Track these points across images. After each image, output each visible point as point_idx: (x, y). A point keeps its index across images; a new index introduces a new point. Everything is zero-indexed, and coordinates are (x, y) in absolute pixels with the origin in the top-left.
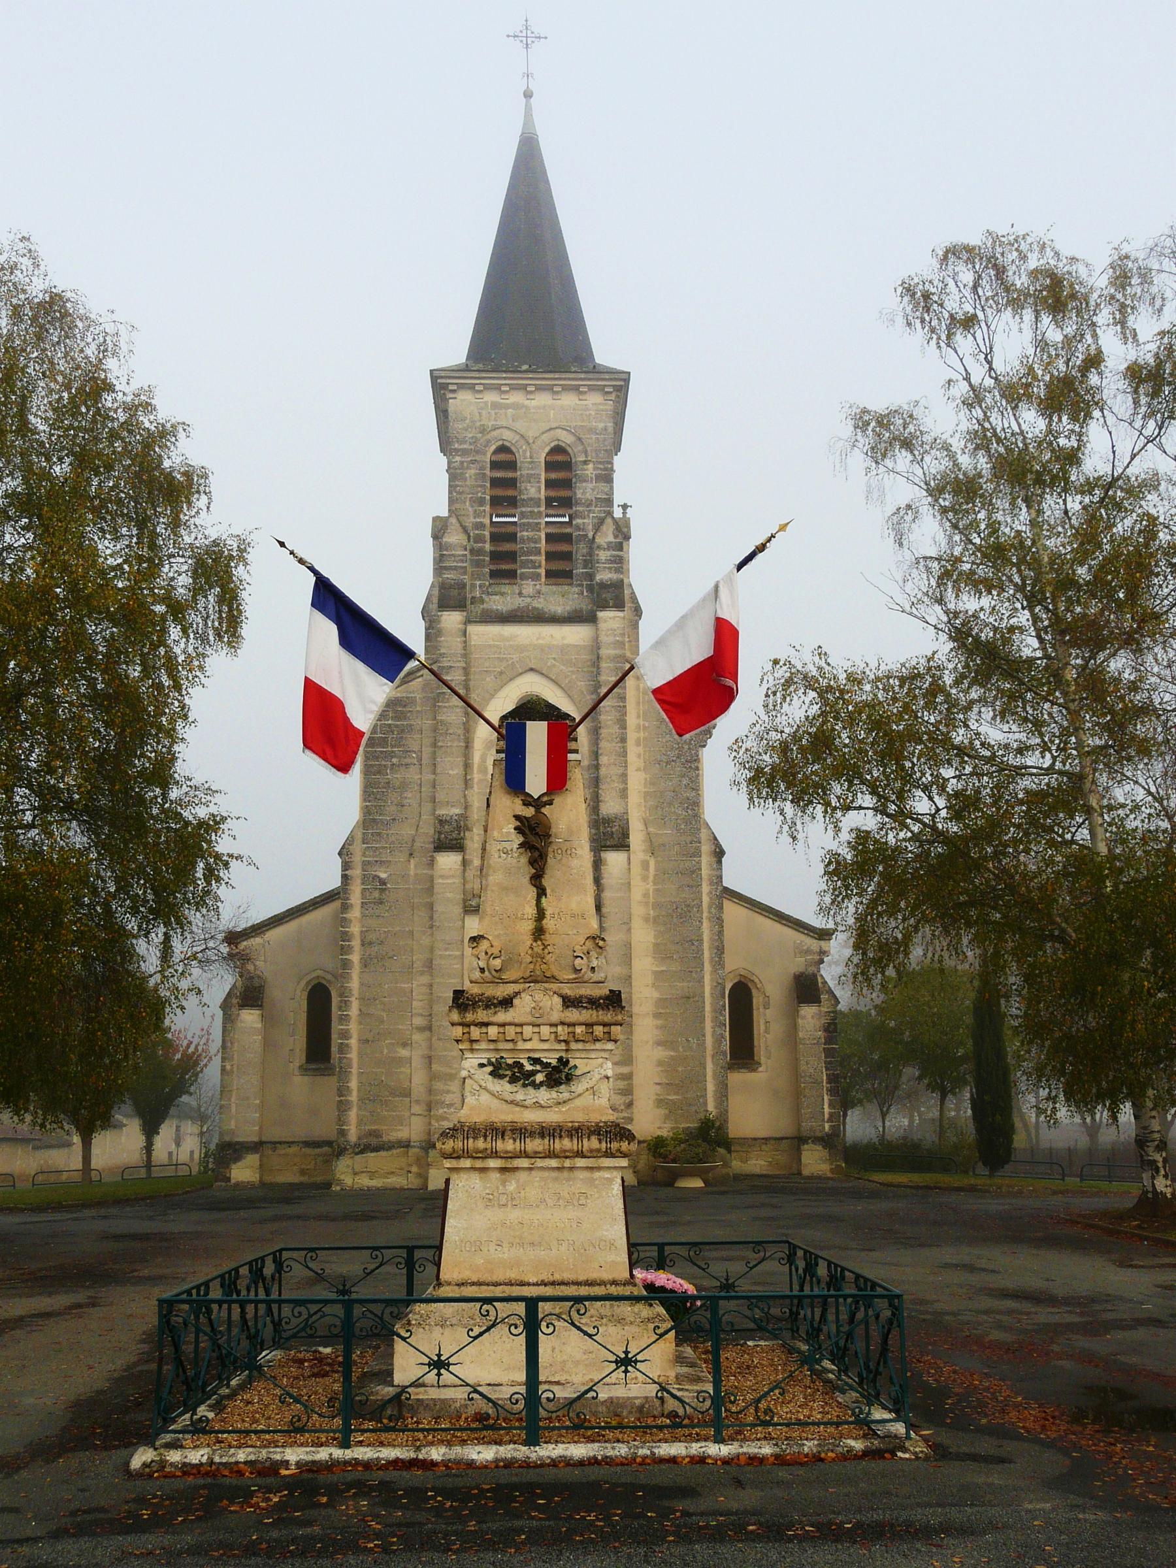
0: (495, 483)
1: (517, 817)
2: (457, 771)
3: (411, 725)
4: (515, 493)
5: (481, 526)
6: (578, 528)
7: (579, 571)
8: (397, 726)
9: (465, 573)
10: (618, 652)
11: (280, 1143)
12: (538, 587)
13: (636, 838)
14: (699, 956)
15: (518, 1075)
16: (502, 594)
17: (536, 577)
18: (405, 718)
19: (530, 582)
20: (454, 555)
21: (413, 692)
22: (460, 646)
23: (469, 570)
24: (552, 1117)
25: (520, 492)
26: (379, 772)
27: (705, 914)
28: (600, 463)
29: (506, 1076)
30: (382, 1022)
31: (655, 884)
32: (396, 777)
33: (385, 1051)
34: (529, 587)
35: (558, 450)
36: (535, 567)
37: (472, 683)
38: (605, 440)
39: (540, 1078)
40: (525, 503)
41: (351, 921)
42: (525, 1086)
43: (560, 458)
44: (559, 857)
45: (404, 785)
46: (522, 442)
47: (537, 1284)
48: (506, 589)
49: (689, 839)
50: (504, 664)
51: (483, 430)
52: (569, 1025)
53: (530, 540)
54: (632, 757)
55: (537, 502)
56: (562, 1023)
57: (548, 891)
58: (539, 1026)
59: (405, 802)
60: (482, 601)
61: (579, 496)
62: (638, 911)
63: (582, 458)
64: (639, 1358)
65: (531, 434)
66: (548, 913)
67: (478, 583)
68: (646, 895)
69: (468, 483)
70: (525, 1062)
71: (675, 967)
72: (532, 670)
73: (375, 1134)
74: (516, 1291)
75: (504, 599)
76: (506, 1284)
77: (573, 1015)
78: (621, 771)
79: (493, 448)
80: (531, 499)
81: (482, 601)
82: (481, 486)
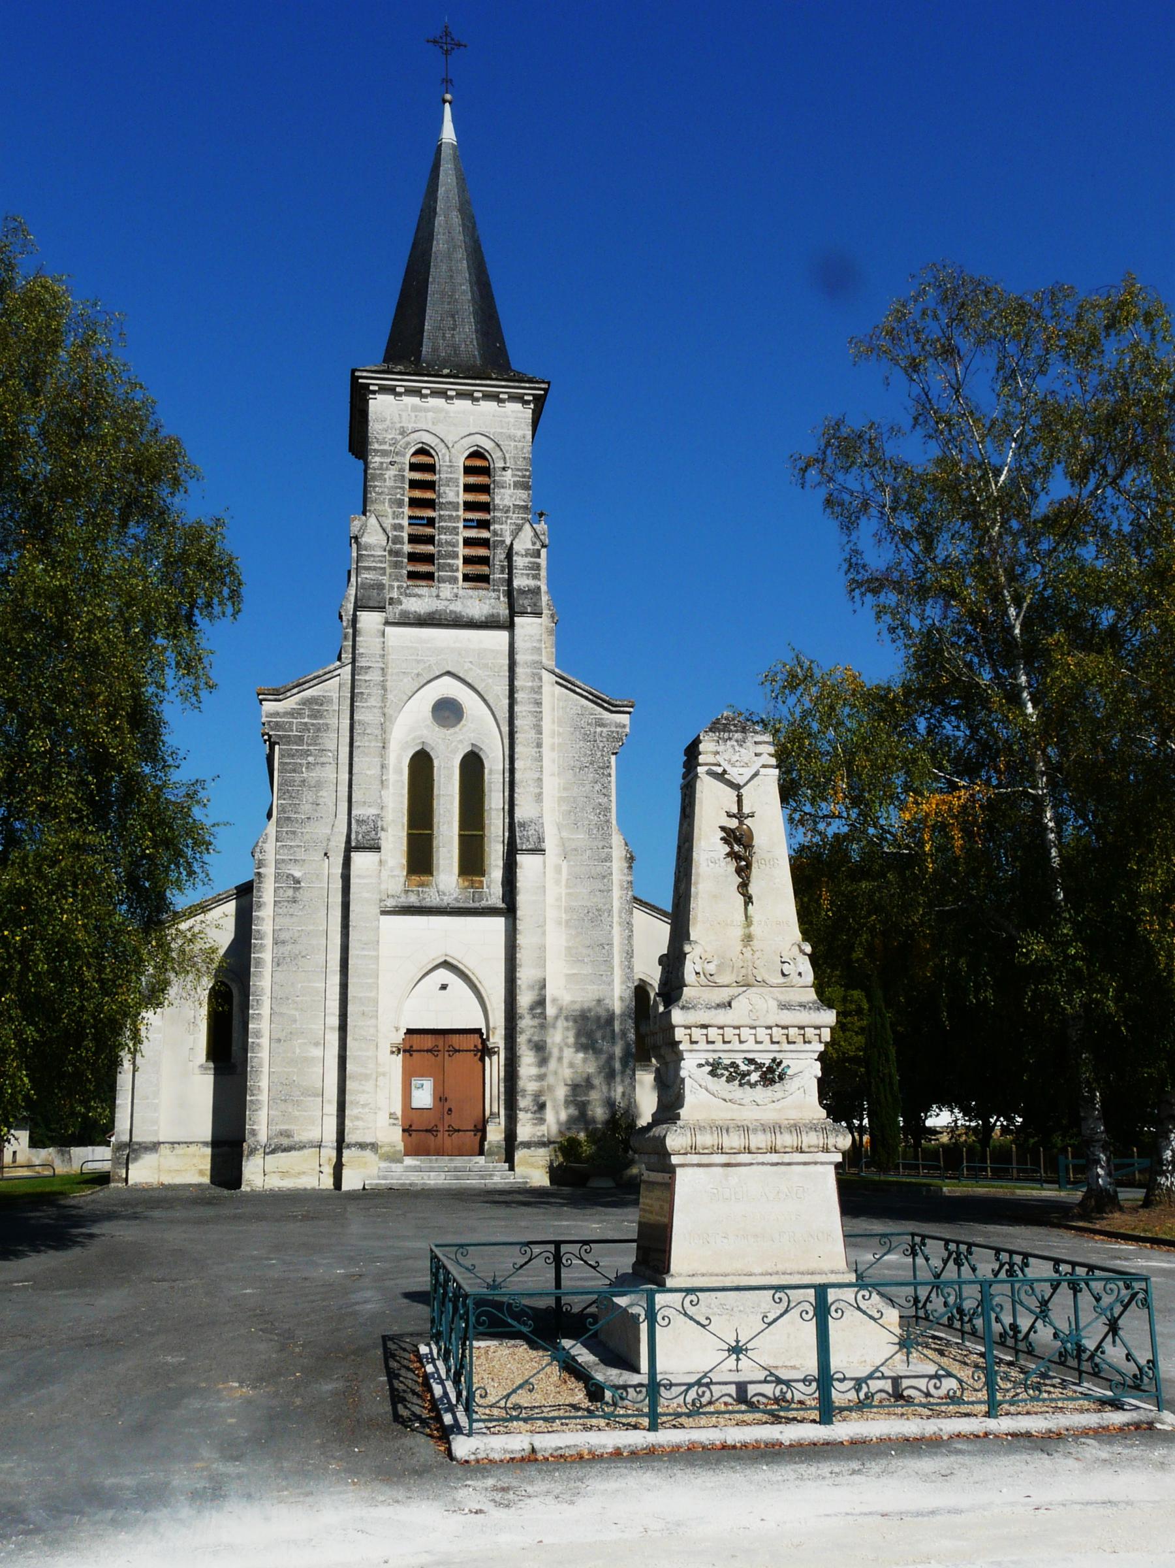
0: (414, 484)
1: (723, 828)
2: (375, 771)
3: (327, 725)
4: (434, 496)
5: (399, 527)
6: (495, 533)
7: (498, 576)
8: (313, 725)
9: (384, 574)
10: (536, 658)
11: (179, 1143)
12: (455, 590)
13: (550, 844)
14: (608, 962)
15: (736, 1075)
16: (419, 596)
17: (454, 580)
18: (321, 717)
19: (447, 585)
20: (372, 556)
21: (330, 691)
22: (380, 646)
23: (388, 571)
24: (769, 1114)
25: (439, 496)
26: (294, 771)
27: (616, 919)
28: (518, 470)
29: (722, 1075)
30: (295, 1021)
31: (568, 887)
32: (312, 776)
33: (298, 1051)
34: (446, 590)
35: (477, 454)
36: (453, 571)
37: (388, 684)
38: (523, 447)
39: (755, 1077)
40: (443, 506)
41: (263, 919)
42: (741, 1085)
43: (479, 463)
44: (762, 867)
45: (319, 785)
46: (442, 445)
47: (762, 1274)
48: (423, 591)
49: (601, 844)
50: (422, 666)
51: (403, 432)
52: (784, 1027)
53: (448, 543)
54: (546, 762)
55: (455, 506)
56: (777, 1026)
57: (754, 900)
58: (755, 1028)
59: (321, 801)
60: (400, 603)
61: (497, 501)
62: (551, 914)
63: (501, 465)
64: (749, 1346)
65: (450, 440)
66: (755, 920)
67: (396, 584)
68: (559, 899)
69: (387, 484)
70: (739, 1062)
71: (587, 970)
72: (448, 673)
73: (287, 1134)
74: (807, 1280)
75: (421, 601)
76: (734, 1275)
77: (787, 1017)
78: (537, 775)
79: (413, 450)
80: (450, 503)
81: (400, 603)
82: (400, 488)
